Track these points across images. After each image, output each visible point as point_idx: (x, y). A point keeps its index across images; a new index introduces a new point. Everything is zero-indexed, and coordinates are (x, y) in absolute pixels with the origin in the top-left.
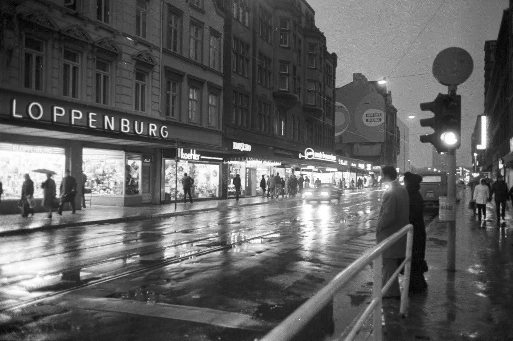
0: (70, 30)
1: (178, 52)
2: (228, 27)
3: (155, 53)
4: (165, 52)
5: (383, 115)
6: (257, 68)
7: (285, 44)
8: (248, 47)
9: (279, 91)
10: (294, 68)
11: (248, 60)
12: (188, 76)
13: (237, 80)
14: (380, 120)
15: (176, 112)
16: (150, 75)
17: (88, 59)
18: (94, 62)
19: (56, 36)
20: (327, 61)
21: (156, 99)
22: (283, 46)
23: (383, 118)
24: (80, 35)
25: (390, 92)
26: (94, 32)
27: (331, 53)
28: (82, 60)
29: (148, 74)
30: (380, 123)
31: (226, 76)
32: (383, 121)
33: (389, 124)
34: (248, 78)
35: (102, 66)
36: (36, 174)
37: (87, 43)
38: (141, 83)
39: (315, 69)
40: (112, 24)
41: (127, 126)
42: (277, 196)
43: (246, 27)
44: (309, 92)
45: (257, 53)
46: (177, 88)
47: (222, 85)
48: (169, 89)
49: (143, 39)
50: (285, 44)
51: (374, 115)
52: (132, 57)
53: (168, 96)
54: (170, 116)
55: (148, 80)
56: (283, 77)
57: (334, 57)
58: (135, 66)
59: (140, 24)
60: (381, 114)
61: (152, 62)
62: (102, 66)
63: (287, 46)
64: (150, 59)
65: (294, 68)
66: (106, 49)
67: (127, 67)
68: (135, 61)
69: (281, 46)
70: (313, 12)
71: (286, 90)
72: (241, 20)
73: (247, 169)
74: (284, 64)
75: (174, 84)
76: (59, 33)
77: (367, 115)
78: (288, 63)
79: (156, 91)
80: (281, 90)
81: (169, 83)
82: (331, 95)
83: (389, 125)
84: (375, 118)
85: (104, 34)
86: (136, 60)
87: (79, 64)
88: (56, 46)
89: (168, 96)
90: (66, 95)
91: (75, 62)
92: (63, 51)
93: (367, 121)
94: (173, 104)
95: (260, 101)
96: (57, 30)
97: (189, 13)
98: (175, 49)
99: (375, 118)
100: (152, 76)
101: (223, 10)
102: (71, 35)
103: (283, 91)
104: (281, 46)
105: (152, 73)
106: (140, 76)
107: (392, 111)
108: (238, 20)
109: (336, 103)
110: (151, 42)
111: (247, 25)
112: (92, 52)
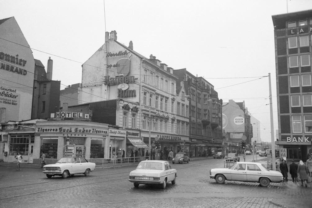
4: (177, 115)
5: (244, 119)
8: (195, 107)
10: (209, 111)
11: (195, 112)
13: (193, 119)
20: (198, 91)
23: (244, 120)
25: (151, 56)
27: (220, 100)
30: (243, 123)
31: (190, 119)
32: (244, 122)
34: (195, 117)
39: (215, 109)
41: (290, 139)
42: (111, 145)
44: (213, 117)
47: (189, 121)
56: (205, 115)
63: (215, 108)
65: (209, 111)
67: (170, 121)
70: (213, 86)
73: (282, 141)
74: (205, 110)
77: (242, 122)
82: (221, 116)
93: (236, 122)
107: (248, 117)
110: (244, 127)
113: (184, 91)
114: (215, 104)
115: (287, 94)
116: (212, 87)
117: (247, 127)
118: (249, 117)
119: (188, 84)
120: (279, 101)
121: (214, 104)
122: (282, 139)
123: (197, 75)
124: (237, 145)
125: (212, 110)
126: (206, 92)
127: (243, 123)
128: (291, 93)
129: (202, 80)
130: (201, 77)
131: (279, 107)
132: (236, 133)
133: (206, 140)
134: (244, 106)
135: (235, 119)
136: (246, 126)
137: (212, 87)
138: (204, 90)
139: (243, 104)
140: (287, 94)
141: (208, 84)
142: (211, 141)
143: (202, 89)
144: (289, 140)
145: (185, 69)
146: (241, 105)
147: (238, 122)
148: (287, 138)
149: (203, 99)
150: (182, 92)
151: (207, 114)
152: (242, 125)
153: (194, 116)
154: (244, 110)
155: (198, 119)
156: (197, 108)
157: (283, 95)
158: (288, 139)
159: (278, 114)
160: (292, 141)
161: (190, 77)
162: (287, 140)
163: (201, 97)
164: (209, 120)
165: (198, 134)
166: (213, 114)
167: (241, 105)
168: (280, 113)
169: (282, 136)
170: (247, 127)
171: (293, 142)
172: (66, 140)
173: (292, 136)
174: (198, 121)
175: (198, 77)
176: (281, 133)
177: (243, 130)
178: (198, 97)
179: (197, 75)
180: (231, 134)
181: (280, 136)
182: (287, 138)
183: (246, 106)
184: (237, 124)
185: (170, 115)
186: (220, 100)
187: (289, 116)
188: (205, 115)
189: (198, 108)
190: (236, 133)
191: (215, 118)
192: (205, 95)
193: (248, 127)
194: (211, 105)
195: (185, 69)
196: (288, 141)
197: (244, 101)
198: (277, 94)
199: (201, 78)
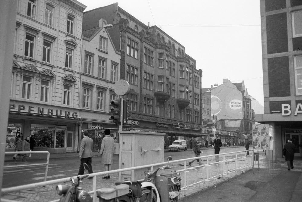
0: (27, 67)
1: (91, 74)
2: (123, 60)
3: (77, 75)
6: (143, 80)
7: (162, 66)
8: (199, 95)
9: (158, 91)
10: (167, 79)
12: (109, 89)
14: (240, 106)
15: (89, 105)
16: (52, 82)
17: (36, 80)
18: (40, 81)
19: (19, 70)
21: (77, 98)
22: (160, 67)
23: (242, 104)
24: (31, 69)
26: (23, 62)
27: (198, 70)
28: (50, 84)
29: (72, 86)
30: (240, 108)
32: (242, 106)
33: (246, 107)
34: (137, 86)
35: (45, 82)
36: (233, 85)
37: (36, 73)
38: (67, 91)
39: (184, 79)
40: (51, 63)
41: (288, 109)
43: (136, 59)
44: (181, 91)
45: (143, 72)
46: (90, 92)
48: (99, 96)
49: (69, 69)
50: (162, 66)
51: (236, 103)
52: (62, 78)
53: (84, 97)
54: (86, 107)
55: (72, 89)
56: (161, 84)
57: (200, 71)
58: (64, 82)
59: (68, 60)
60: (240, 102)
61: (74, 79)
62: (45, 82)
63: (163, 67)
64: (73, 78)
66: (47, 75)
68: (64, 80)
69: (160, 67)
70: (184, 48)
71: (163, 91)
72: (132, 55)
73: (271, 113)
74: (161, 77)
75: (88, 91)
76: (21, 68)
77: (232, 103)
78: (163, 77)
79: (77, 94)
80: (159, 91)
81: (85, 90)
83: (246, 109)
84: (237, 104)
85: (46, 67)
86: (64, 79)
87: (49, 86)
88: (38, 79)
89: (84, 97)
90: (29, 99)
91: (47, 85)
92: (41, 81)
93: (232, 106)
94: (88, 100)
95: (173, 105)
96: (19, 67)
97: (97, 54)
98: (89, 73)
99: (237, 104)
100: (74, 87)
101: (120, 51)
102: (27, 69)
103: (161, 92)
104: (160, 67)
105: (74, 85)
106: (67, 87)
108: (130, 56)
109: (211, 96)
111: (136, 57)
112: (39, 76)
113: (106, 35)
114: (184, 71)
115: (284, 10)
116: (181, 48)
117: (246, 112)
118: (250, 100)
119: (120, 29)
120: (265, 27)
121: (182, 72)
122: (271, 109)
123: (149, 23)
124: (229, 135)
125: (179, 80)
126: (163, 49)
127: (240, 108)
128: (292, 6)
129: (157, 31)
130: (156, 26)
131: (266, 45)
132: (232, 120)
133: (164, 124)
134: (244, 86)
135: (231, 103)
136: (244, 112)
137: (183, 49)
138: (159, 46)
139: (242, 85)
140: (284, 10)
141: (172, 41)
142: (177, 126)
143: (156, 44)
144: (286, 112)
145: (117, 4)
146: (239, 87)
147: (235, 107)
148: (283, 105)
149: (158, 61)
150: (102, 37)
151: (163, 83)
152: (241, 109)
153: (197, 104)
154: (243, 92)
155: (194, 106)
156: (193, 92)
157: (274, 12)
158: (283, 110)
159: (263, 55)
160: (293, 113)
161: (123, 17)
162: (281, 112)
163: (153, 55)
164: (168, 92)
165: (189, 122)
166: (181, 86)
167: (239, 87)
168: (266, 53)
169: (272, 103)
170: (246, 112)
171: (296, 114)
172: (96, 131)
173: (293, 103)
174: (195, 108)
175: (150, 26)
176: (271, 96)
177: (241, 117)
178: (195, 81)
179: (149, 23)
180: (226, 121)
181: (268, 103)
182: (283, 105)
183: (247, 86)
184: (233, 108)
185: (20, 59)
186: (198, 70)
187: (287, 58)
188: (161, 84)
189: (195, 94)
190: (232, 120)
191: (184, 91)
192: (161, 55)
193: (248, 112)
194: (178, 73)
195: (117, 4)
196: (283, 114)
197: (243, 82)
198: (261, 13)
199: (155, 27)
